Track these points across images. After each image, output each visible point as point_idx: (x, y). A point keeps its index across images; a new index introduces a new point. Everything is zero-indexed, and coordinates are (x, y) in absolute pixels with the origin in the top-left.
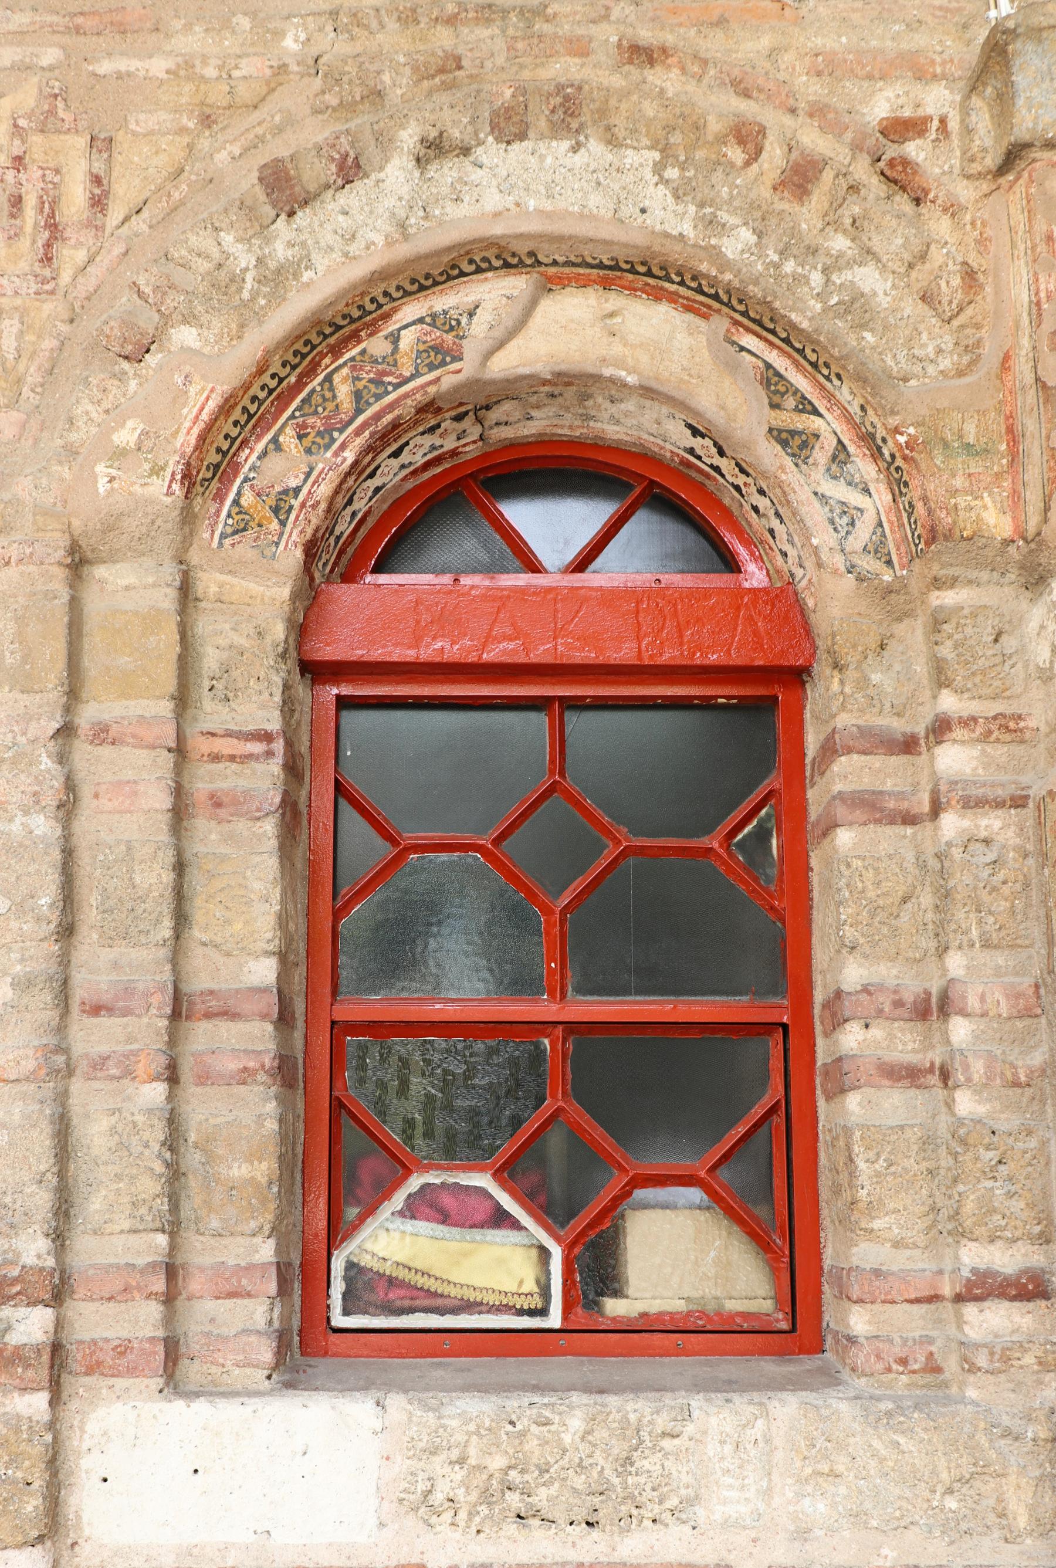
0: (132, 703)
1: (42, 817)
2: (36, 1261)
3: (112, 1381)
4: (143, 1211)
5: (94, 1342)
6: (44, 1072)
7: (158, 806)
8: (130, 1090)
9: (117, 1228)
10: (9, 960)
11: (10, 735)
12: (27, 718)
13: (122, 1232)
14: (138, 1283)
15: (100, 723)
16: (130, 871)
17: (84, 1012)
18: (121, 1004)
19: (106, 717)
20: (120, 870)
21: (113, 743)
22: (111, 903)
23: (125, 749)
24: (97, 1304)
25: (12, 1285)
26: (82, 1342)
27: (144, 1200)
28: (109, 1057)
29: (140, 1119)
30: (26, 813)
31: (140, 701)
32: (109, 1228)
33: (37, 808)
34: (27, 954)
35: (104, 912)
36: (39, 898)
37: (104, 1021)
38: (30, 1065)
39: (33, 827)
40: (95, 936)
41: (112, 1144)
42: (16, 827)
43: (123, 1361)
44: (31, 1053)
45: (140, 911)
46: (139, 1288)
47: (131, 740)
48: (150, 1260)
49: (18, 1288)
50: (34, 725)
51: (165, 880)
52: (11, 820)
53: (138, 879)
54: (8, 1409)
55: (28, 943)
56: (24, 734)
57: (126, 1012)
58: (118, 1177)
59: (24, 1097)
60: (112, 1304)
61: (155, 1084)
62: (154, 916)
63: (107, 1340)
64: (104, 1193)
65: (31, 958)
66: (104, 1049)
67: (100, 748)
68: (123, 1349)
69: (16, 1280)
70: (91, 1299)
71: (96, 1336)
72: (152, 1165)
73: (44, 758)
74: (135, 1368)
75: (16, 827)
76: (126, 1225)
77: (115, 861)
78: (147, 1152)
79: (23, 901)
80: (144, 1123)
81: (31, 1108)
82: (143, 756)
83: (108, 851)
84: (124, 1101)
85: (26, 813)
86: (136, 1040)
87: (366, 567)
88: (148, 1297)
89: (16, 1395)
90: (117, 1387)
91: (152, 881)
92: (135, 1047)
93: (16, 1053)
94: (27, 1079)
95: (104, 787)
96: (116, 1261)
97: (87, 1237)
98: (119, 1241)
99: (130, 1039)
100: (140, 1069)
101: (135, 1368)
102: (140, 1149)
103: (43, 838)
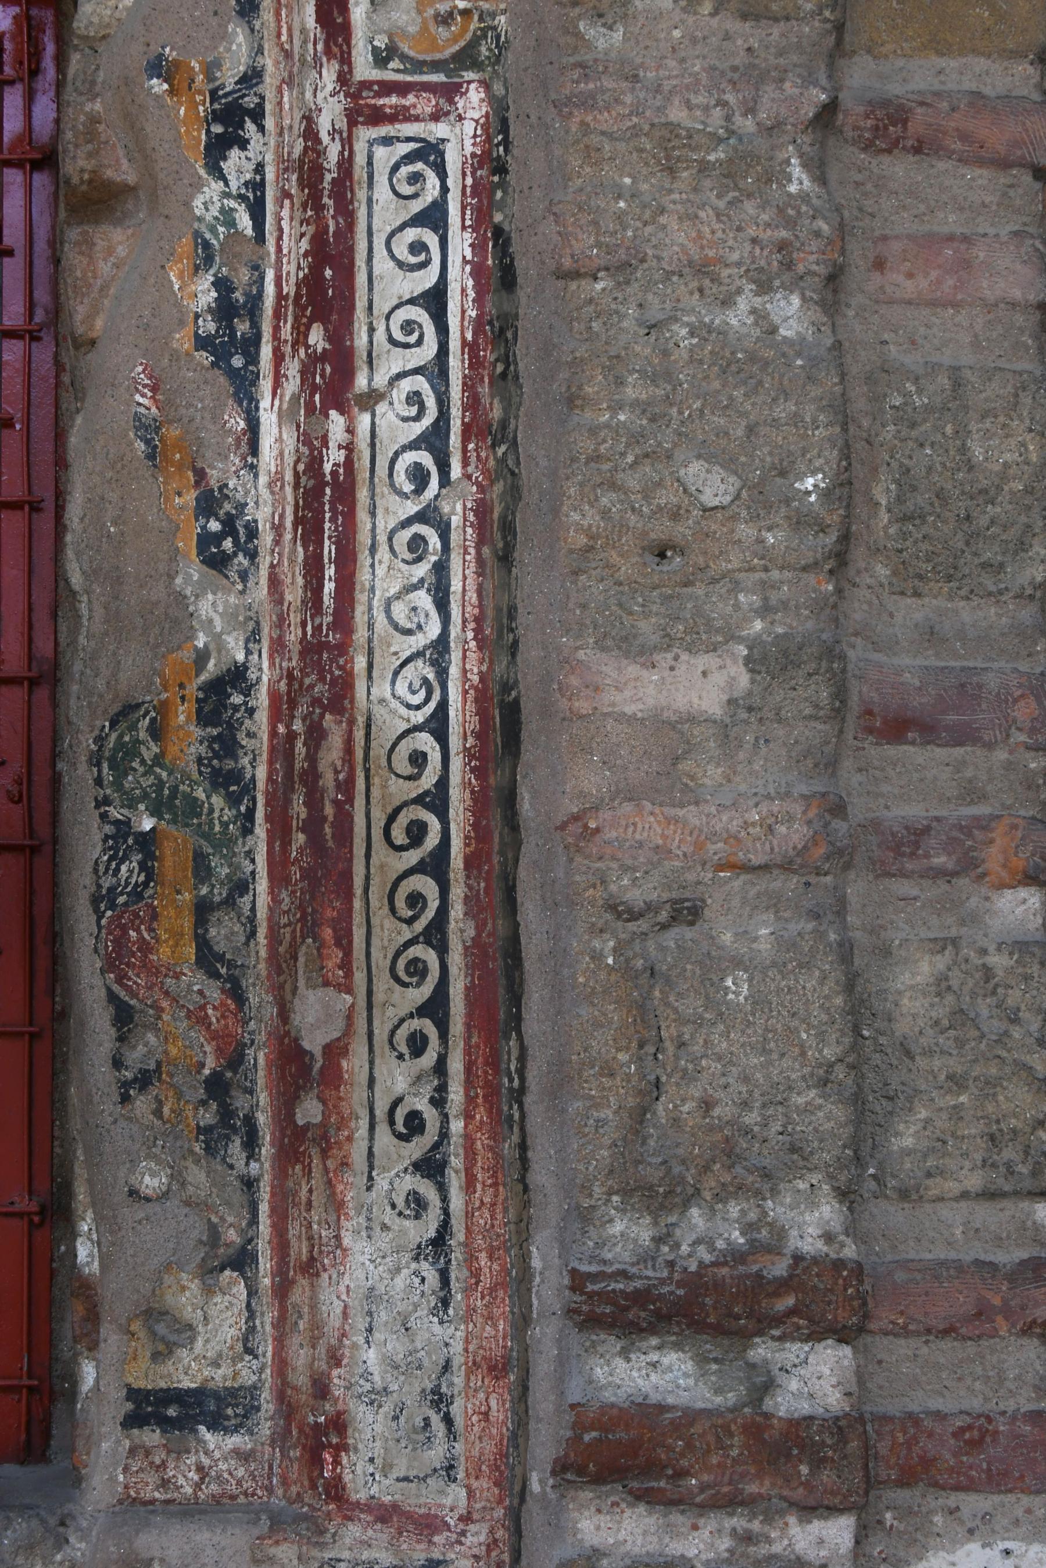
0: (951, 64)
1: (796, 300)
2: (821, 1246)
3: (954, 1499)
4: (1009, 1153)
5: (913, 1419)
6: (821, 851)
7: (1017, 294)
8: (973, 902)
9: (953, 1187)
10: (737, 606)
11: (718, 112)
12: (752, 76)
13: (965, 1195)
14: (1005, 1301)
15: (886, 103)
16: (962, 432)
17: (870, 730)
18: (952, 718)
19: (895, 89)
20: (938, 429)
21: (917, 150)
22: (922, 499)
23: (942, 165)
24: (913, 1342)
25: (776, 1294)
26: (885, 1419)
27: (1014, 1131)
28: (927, 830)
29: (999, 961)
30: (764, 287)
31: (970, 59)
32: (935, 1187)
33: (787, 277)
34: (774, 597)
35: (906, 518)
36: (801, 477)
37: (912, 753)
38: (794, 834)
39: (776, 320)
40: (882, 571)
41: (940, 1012)
42: (738, 317)
43: (980, 1459)
44: (797, 809)
45: (984, 521)
46: (1006, 1311)
47: (958, 146)
48: (1025, 1256)
49: (790, 1301)
50: (769, 92)
51: (1034, 458)
52: (727, 302)
53: (978, 454)
54: (777, 1548)
55: (775, 574)
56: (750, 110)
57: (963, 736)
58: (957, 1082)
59: (774, 903)
60: (947, 1344)
61: (1023, 893)
62: (1013, 533)
63: (939, 1416)
64: (923, 1114)
65: (785, 605)
66: (915, 811)
67: (886, 159)
68: (976, 1434)
69: (783, 1285)
70: (905, 1332)
71: (914, 1407)
72: (1028, 1059)
73: (796, 170)
74: (1005, 1474)
75: (738, 317)
76: (974, 1181)
77: (929, 409)
78: (1016, 1033)
79: (763, 480)
80: (1009, 971)
81: (794, 927)
82: (978, 182)
83: (910, 387)
84: (962, 923)
85: (764, 287)
86: (984, 797)
87: (13, 38)
88: (1026, 1331)
89: (792, 1520)
90: (965, 1512)
91: (1008, 457)
92: (982, 810)
93: (764, 808)
94: (787, 867)
95: (896, 246)
96: (953, 1255)
97: (883, 1203)
98: (955, 1215)
99: (972, 793)
100: (993, 858)
101: (1005, 1474)
102: (997, 1025)
103: (798, 345)
